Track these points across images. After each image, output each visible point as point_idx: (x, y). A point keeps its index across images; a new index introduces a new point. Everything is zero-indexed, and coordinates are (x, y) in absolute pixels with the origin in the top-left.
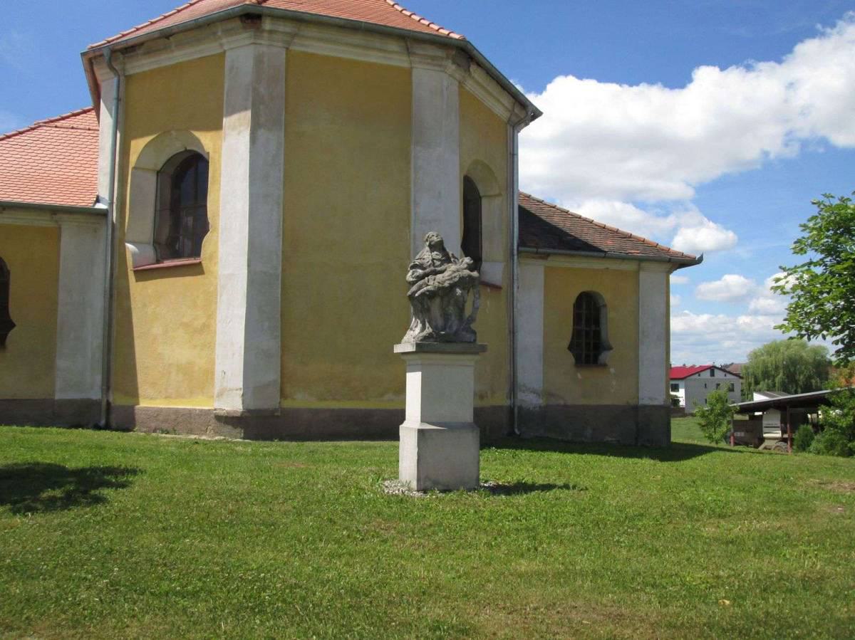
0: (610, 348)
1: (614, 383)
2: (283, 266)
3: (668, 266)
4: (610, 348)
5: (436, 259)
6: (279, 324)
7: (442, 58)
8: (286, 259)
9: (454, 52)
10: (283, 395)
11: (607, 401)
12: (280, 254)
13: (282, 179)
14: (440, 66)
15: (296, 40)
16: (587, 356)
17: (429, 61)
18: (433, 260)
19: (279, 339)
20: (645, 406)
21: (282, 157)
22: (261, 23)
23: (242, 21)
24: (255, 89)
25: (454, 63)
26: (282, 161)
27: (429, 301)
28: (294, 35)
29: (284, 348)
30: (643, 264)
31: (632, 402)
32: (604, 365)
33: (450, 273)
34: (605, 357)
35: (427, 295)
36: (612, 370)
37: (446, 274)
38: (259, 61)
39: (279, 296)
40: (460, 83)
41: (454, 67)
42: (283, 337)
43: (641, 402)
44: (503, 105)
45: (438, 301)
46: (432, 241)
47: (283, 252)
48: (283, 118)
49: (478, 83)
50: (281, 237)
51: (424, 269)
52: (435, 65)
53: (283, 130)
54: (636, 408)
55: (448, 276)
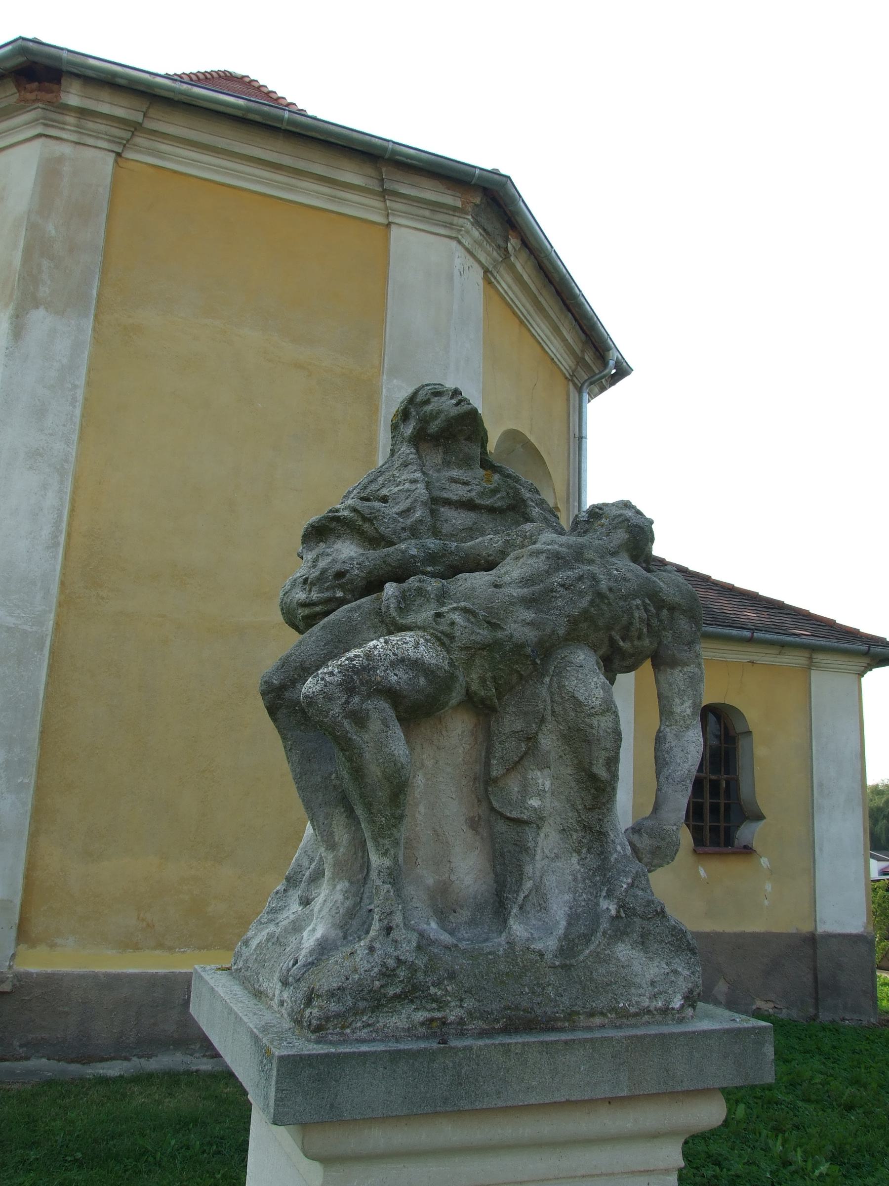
0: (759, 817)
1: (768, 887)
2: (58, 615)
3: (864, 661)
4: (759, 817)
5: (448, 502)
6: (34, 758)
7: (455, 209)
8: (67, 601)
9: (478, 201)
10: (23, 933)
11: (756, 926)
12: (55, 589)
13: (77, 420)
14: (449, 225)
15: (139, 140)
16: (715, 830)
17: (427, 213)
18: (436, 502)
19: (28, 797)
20: (829, 937)
21: (84, 370)
22: (59, 91)
23: (18, 86)
24: (32, 227)
25: (477, 223)
26: (82, 382)
27: (397, 731)
28: (136, 128)
29: (41, 815)
30: (817, 657)
31: (805, 928)
32: (747, 850)
33: (540, 564)
34: (747, 833)
35: (391, 695)
36: (764, 862)
37: (512, 570)
38: (49, 174)
39: (43, 687)
40: (486, 271)
41: (476, 233)
42: (40, 791)
43: (821, 929)
44: (564, 340)
45: (457, 732)
46: (434, 416)
47: (62, 583)
48: (95, 292)
49: (519, 279)
50: (61, 550)
51: (376, 541)
52: (439, 223)
53: (92, 317)
54: (812, 940)
55: (527, 581)
